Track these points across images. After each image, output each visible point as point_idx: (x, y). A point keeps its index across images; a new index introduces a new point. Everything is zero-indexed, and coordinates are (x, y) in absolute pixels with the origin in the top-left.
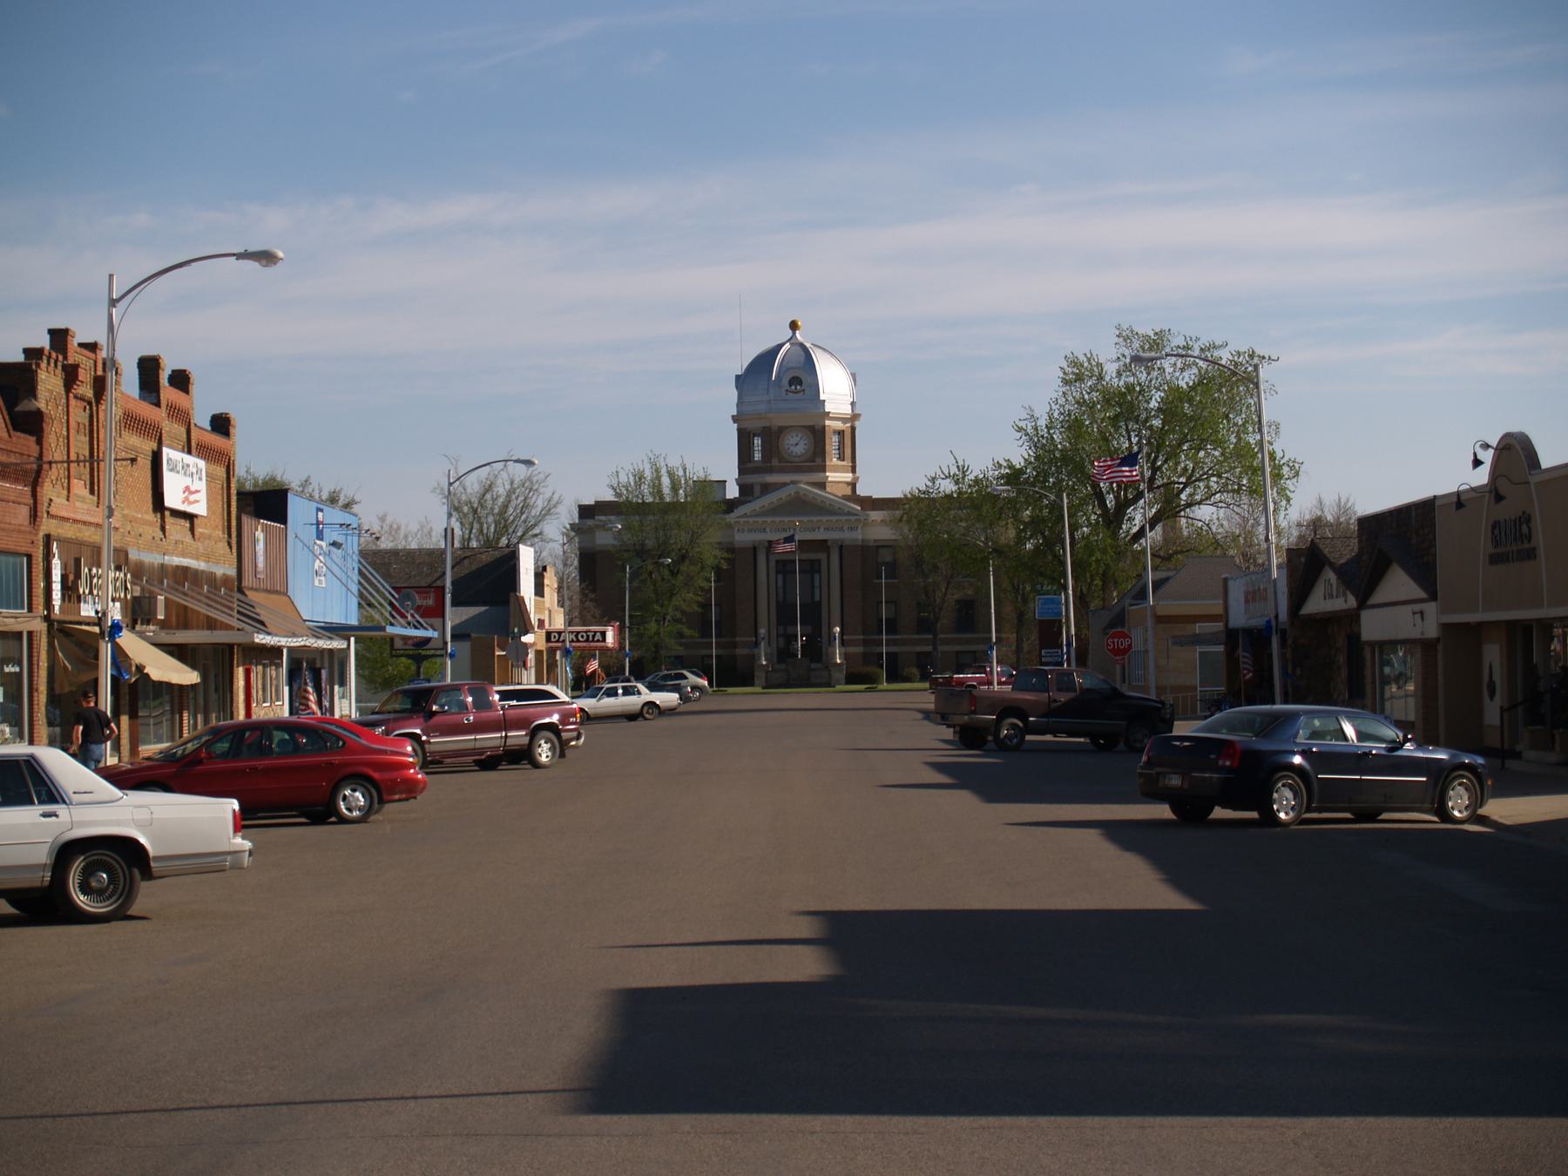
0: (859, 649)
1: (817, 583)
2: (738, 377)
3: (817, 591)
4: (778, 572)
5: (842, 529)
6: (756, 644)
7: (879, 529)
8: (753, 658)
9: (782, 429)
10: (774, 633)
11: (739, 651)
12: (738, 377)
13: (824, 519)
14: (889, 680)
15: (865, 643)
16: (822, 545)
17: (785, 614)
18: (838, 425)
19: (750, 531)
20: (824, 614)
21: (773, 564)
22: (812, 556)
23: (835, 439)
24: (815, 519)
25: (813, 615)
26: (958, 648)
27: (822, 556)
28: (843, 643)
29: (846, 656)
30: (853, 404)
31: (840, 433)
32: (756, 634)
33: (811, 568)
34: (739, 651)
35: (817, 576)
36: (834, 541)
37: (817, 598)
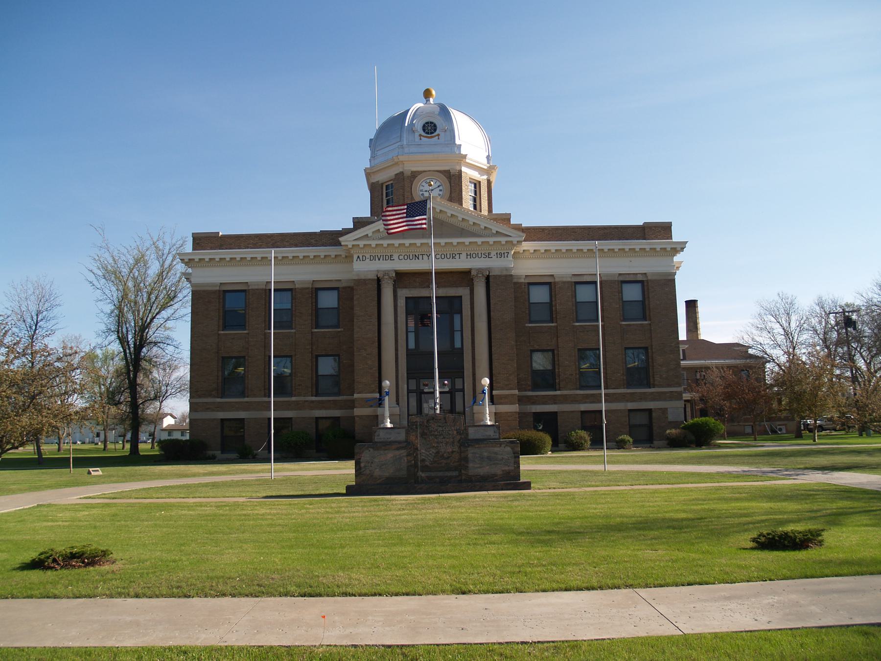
0: (514, 408)
1: (457, 326)
2: (371, 140)
3: (457, 336)
4: (408, 313)
5: (488, 256)
6: (380, 403)
7: (530, 263)
8: (376, 420)
9: (415, 175)
10: (404, 387)
11: (358, 412)
12: (371, 140)
13: (467, 241)
14: (553, 451)
15: (521, 400)
16: (465, 277)
17: (418, 367)
18: (476, 175)
19: (373, 258)
20: (467, 365)
21: (402, 303)
22: (452, 292)
23: (472, 187)
24: (455, 241)
25: (454, 366)
26: (631, 406)
27: (463, 292)
28: (492, 400)
29: (497, 416)
30: (488, 157)
31: (477, 185)
32: (380, 389)
33: (451, 307)
34: (358, 412)
35: (457, 318)
36: (480, 271)
37: (458, 345)
